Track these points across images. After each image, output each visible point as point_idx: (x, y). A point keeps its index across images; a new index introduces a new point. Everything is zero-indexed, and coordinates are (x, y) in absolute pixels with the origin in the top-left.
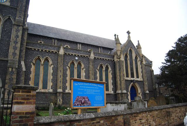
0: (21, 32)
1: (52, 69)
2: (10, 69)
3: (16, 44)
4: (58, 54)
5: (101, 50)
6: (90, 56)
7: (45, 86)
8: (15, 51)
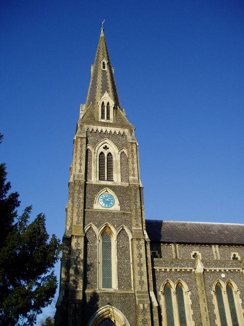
0: (143, 248)
1: (191, 299)
2: (141, 306)
3: (140, 270)
4: (194, 272)
5: (175, 248)
6: (195, 269)
7: (107, 283)
8: (141, 279)
